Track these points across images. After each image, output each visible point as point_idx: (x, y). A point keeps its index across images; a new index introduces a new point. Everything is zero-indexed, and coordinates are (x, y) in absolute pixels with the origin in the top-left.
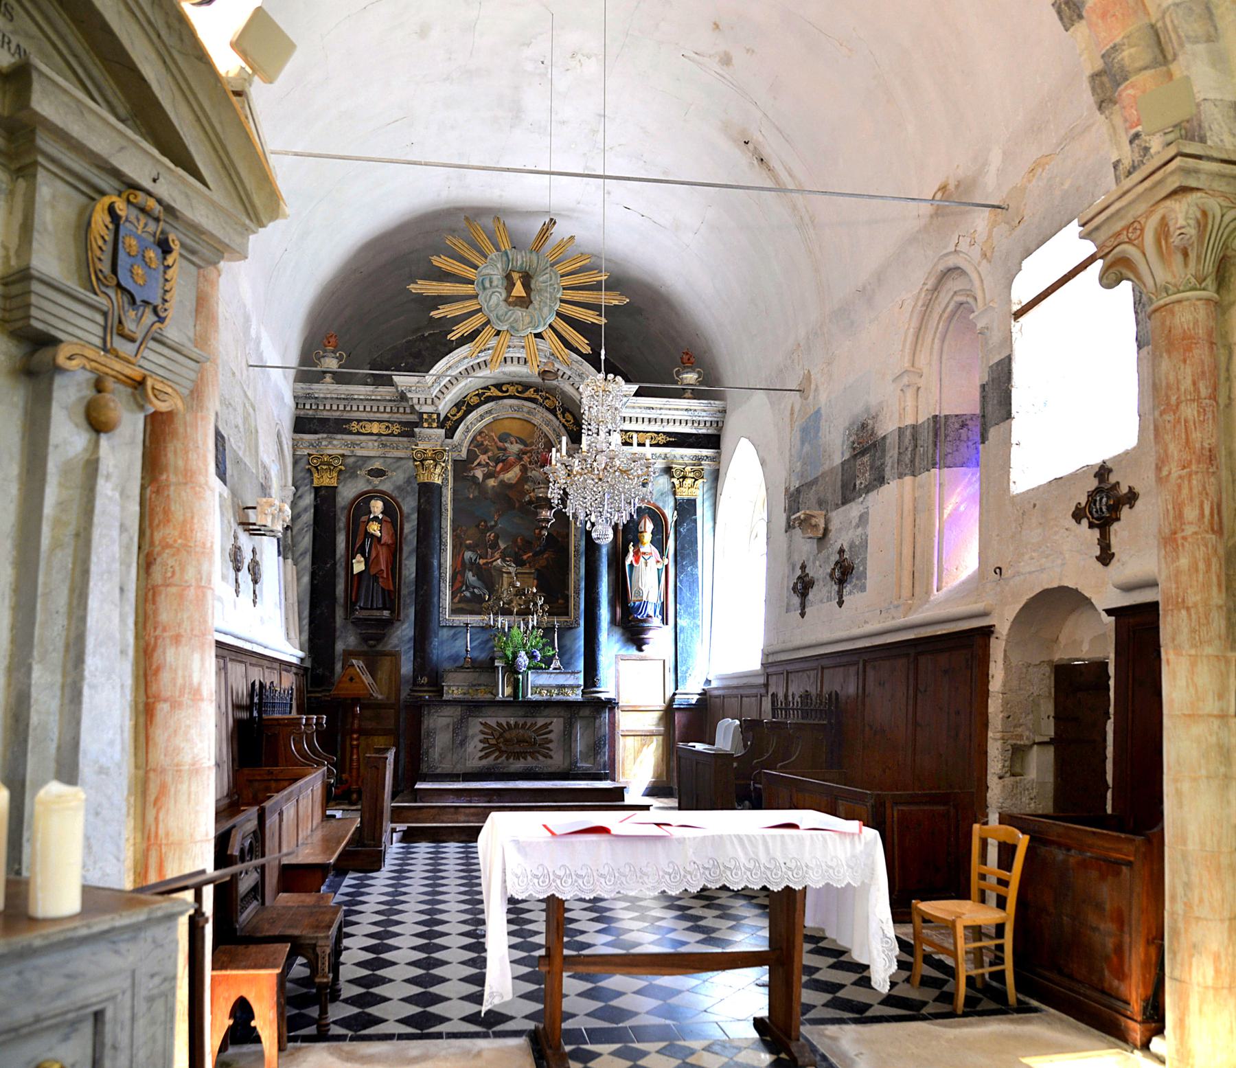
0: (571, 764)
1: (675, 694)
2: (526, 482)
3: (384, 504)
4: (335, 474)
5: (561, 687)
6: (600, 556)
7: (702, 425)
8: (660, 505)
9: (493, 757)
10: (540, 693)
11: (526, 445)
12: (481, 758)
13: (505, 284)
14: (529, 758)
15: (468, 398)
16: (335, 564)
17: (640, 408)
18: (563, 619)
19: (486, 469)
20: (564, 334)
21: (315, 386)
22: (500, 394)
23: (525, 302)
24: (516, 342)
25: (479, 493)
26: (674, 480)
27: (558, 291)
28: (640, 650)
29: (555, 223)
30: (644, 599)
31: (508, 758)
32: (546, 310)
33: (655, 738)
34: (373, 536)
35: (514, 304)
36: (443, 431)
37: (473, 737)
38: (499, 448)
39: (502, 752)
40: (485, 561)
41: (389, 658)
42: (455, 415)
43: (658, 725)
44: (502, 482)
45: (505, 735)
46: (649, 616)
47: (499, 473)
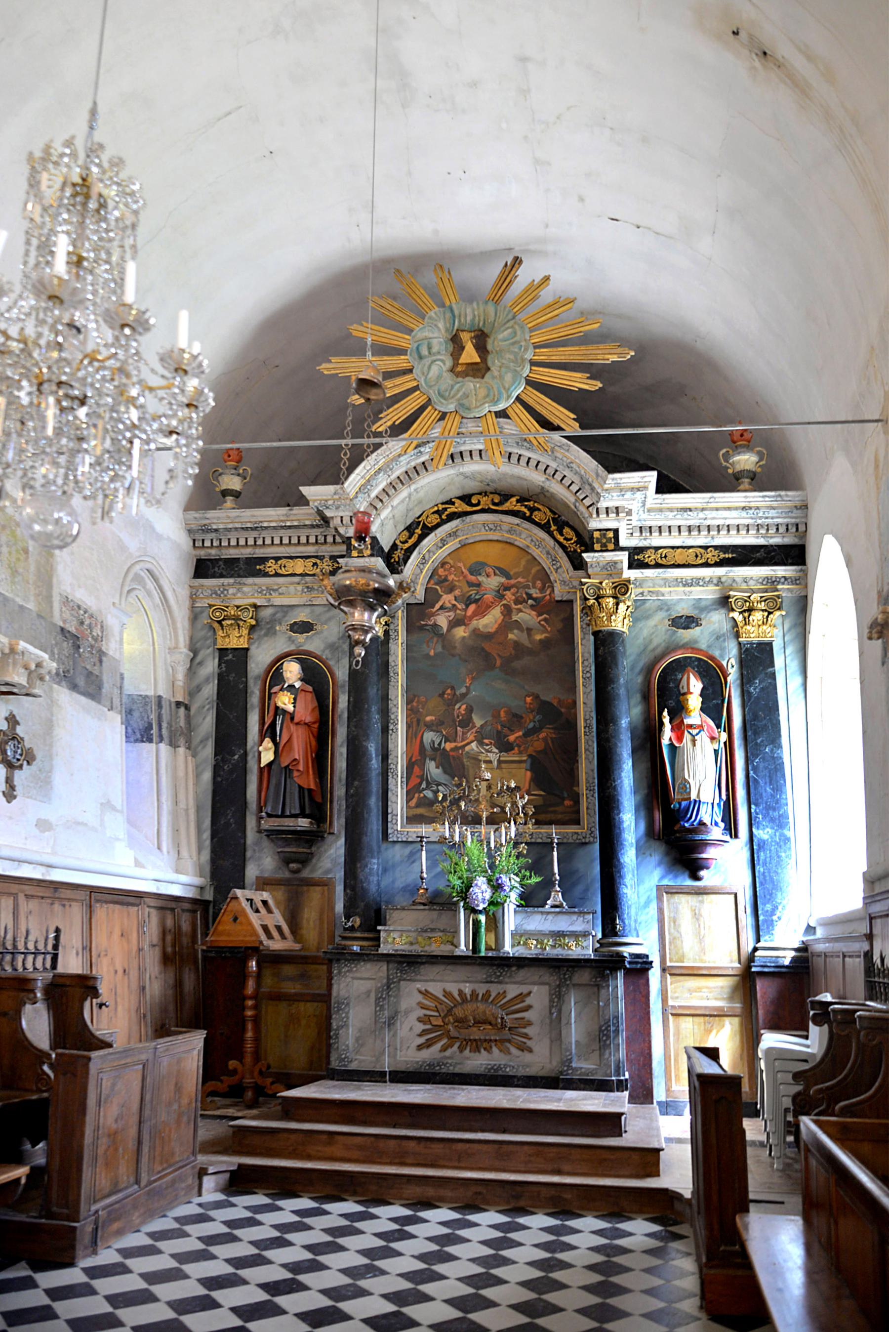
0: (563, 1063)
1: (755, 949)
2: (511, 630)
3: (303, 669)
4: (245, 632)
5: (558, 935)
6: (617, 733)
7: (772, 531)
8: (717, 654)
9: (438, 1046)
10: (525, 944)
11: (508, 576)
12: (420, 1047)
13: (451, 349)
14: (495, 1050)
15: (424, 517)
16: (245, 754)
17: (671, 510)
18: (571, 829)
19: (452, 614)
20: (538, 408)
21: (211, 514)
22: (469, 509)
23: (479, 370)
24: (470, 426)
25: (444, 647)
26: (735, 615)
27: (526, 349)
28: (697, 878)
29: (521, 262)
30: (693, 796)
31: (461, 1049)
32: (508, 377)
33: (727, 1021)
34: (284, 712)
35: (464, 374)
36: (513, 597)
37: (407, 1013)
38: (470, 584)
39: (452, 1039)
40: (453, 745)
41: (318, 889)
42: (406, 542)
43: (731, 998)
44: (476, 632)
45: (455, 1010)
46: (702, 823)
47: (471, 618)
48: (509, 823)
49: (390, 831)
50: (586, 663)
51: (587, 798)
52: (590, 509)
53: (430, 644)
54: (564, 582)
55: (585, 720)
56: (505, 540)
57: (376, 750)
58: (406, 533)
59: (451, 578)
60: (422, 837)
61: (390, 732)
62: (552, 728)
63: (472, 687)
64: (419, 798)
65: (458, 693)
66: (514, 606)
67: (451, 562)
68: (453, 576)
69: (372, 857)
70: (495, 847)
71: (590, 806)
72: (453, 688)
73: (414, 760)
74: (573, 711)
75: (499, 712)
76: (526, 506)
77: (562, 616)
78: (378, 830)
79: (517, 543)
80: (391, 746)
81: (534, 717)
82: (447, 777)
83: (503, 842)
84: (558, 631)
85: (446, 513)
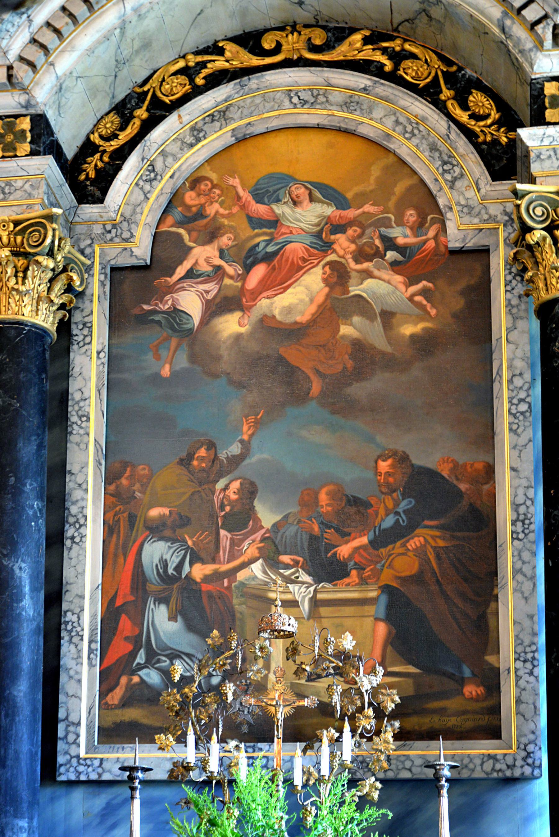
2: (347, 317)
15: (154, 83)
19: (212, 288)
22: (256, 61)
25: (193, 358)
36: (353, 247)
40: (209, 569)
47: (255, 294)
48: (340, 731)
49: (61, 759)
50: (518, 382)
51: (518, 678)
52: (539, 28)
53: (164, 353)
54: (468, 209)
55: (516, 507)
56: (335, 123)
57: (34, 578)
58: (114, 118)
59: (211, 210)
60: (132, 769)
61: (68, 543)
62: (437, 527)
63: (255, 443)
64: (130, 687)
65: (222, 456)
66: (352, 264)
67: (214, 176)
68: (216, 206)
69: (17, 815)
70: (305, 786)
71: (525, 696)
72: (211, 445)
73: (118, 603)
74: (486, 487)
75: (317, 494)
76: (384, 51)
77: (463, 284)
78: (32, 756)
79: (363, 130)
80: (68, 574)
81: (397, 505)
82: (193, 638)
83: (325, 770)
84: (455, 316)
85: (205, 72)
